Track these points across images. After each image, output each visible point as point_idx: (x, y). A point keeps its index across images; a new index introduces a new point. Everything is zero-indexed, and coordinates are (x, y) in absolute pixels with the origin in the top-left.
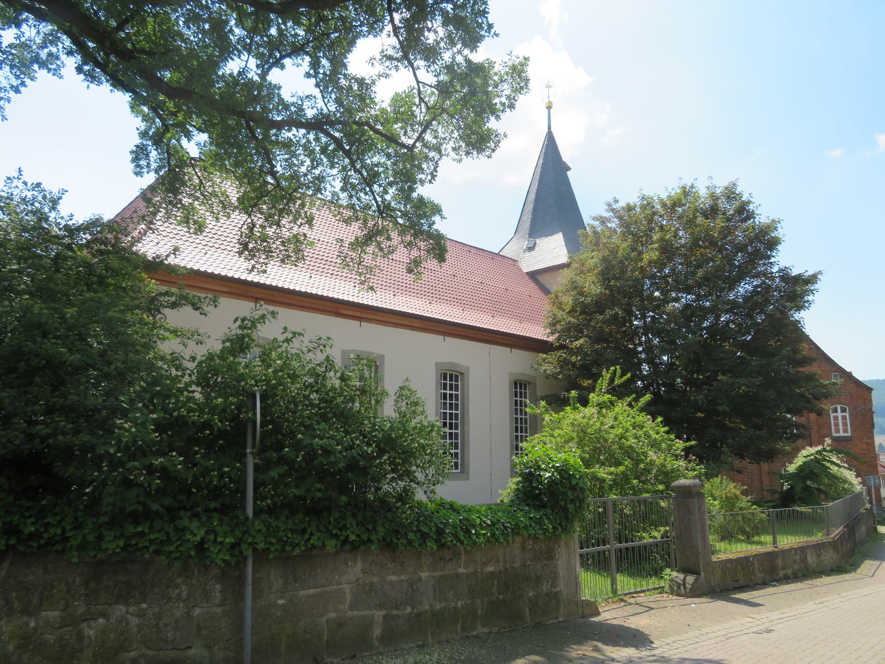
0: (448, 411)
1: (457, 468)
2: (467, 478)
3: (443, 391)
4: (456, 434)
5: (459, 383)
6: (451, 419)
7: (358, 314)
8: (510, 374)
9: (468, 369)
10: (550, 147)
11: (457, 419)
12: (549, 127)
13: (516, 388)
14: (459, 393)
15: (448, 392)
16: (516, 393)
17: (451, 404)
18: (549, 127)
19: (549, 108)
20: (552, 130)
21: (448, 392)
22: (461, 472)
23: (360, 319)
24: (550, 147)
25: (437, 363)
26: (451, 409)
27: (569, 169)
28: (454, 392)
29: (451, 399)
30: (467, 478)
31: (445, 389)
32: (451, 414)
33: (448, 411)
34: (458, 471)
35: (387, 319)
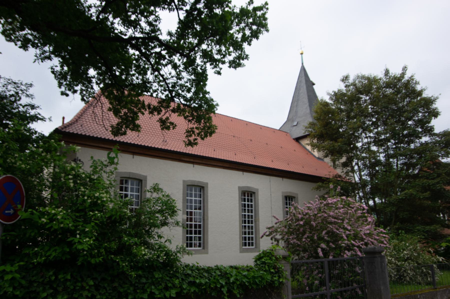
0: (247, 214)
1: (252, 245)
2: (207, 253)
3: (243, 203)
4: (252, 216)
5: (254, 230)
6: (248, 218)
7: (192, 160)
8: (283, 192)
9: (258, 190)
10: (303, 70)
11: (252, 218)
12: (302, 64)
13: (286, 200)
14: (253, 214)
15: (246, 203)
16: (287, 203)
17: (248, 210)
18: (302, 64)
19: (302, 54)
20: (304, 64)
21: (246, 203)
22: (256, 247)
23: (193, 163)
24: (303, 70)
25: (239, 187)
26: (248, 212)
27: (314, 84)
28: (250, 203)
29: (248, 207)
30: (207, 253)
31: (245, 201)
32: (248, 205)
33: (247, 214)
34: (254, 247)
35: (209, 163)
